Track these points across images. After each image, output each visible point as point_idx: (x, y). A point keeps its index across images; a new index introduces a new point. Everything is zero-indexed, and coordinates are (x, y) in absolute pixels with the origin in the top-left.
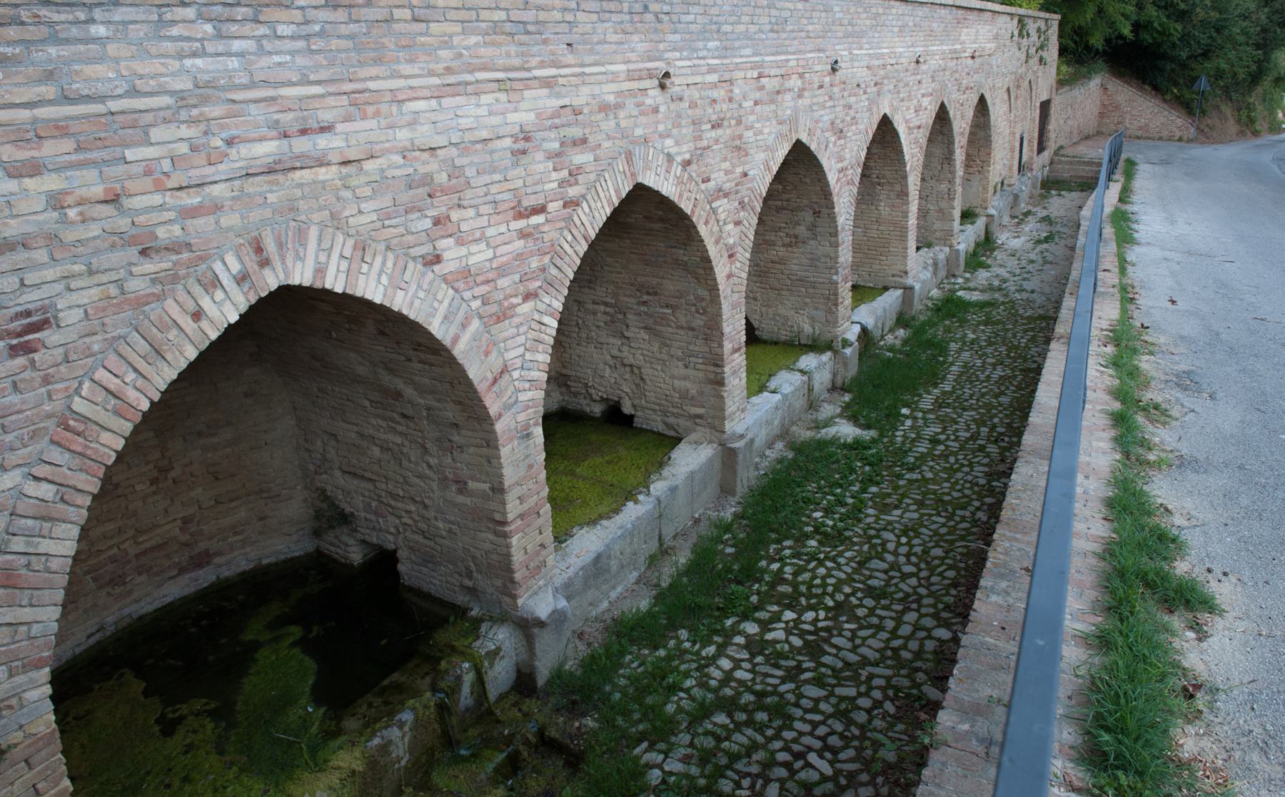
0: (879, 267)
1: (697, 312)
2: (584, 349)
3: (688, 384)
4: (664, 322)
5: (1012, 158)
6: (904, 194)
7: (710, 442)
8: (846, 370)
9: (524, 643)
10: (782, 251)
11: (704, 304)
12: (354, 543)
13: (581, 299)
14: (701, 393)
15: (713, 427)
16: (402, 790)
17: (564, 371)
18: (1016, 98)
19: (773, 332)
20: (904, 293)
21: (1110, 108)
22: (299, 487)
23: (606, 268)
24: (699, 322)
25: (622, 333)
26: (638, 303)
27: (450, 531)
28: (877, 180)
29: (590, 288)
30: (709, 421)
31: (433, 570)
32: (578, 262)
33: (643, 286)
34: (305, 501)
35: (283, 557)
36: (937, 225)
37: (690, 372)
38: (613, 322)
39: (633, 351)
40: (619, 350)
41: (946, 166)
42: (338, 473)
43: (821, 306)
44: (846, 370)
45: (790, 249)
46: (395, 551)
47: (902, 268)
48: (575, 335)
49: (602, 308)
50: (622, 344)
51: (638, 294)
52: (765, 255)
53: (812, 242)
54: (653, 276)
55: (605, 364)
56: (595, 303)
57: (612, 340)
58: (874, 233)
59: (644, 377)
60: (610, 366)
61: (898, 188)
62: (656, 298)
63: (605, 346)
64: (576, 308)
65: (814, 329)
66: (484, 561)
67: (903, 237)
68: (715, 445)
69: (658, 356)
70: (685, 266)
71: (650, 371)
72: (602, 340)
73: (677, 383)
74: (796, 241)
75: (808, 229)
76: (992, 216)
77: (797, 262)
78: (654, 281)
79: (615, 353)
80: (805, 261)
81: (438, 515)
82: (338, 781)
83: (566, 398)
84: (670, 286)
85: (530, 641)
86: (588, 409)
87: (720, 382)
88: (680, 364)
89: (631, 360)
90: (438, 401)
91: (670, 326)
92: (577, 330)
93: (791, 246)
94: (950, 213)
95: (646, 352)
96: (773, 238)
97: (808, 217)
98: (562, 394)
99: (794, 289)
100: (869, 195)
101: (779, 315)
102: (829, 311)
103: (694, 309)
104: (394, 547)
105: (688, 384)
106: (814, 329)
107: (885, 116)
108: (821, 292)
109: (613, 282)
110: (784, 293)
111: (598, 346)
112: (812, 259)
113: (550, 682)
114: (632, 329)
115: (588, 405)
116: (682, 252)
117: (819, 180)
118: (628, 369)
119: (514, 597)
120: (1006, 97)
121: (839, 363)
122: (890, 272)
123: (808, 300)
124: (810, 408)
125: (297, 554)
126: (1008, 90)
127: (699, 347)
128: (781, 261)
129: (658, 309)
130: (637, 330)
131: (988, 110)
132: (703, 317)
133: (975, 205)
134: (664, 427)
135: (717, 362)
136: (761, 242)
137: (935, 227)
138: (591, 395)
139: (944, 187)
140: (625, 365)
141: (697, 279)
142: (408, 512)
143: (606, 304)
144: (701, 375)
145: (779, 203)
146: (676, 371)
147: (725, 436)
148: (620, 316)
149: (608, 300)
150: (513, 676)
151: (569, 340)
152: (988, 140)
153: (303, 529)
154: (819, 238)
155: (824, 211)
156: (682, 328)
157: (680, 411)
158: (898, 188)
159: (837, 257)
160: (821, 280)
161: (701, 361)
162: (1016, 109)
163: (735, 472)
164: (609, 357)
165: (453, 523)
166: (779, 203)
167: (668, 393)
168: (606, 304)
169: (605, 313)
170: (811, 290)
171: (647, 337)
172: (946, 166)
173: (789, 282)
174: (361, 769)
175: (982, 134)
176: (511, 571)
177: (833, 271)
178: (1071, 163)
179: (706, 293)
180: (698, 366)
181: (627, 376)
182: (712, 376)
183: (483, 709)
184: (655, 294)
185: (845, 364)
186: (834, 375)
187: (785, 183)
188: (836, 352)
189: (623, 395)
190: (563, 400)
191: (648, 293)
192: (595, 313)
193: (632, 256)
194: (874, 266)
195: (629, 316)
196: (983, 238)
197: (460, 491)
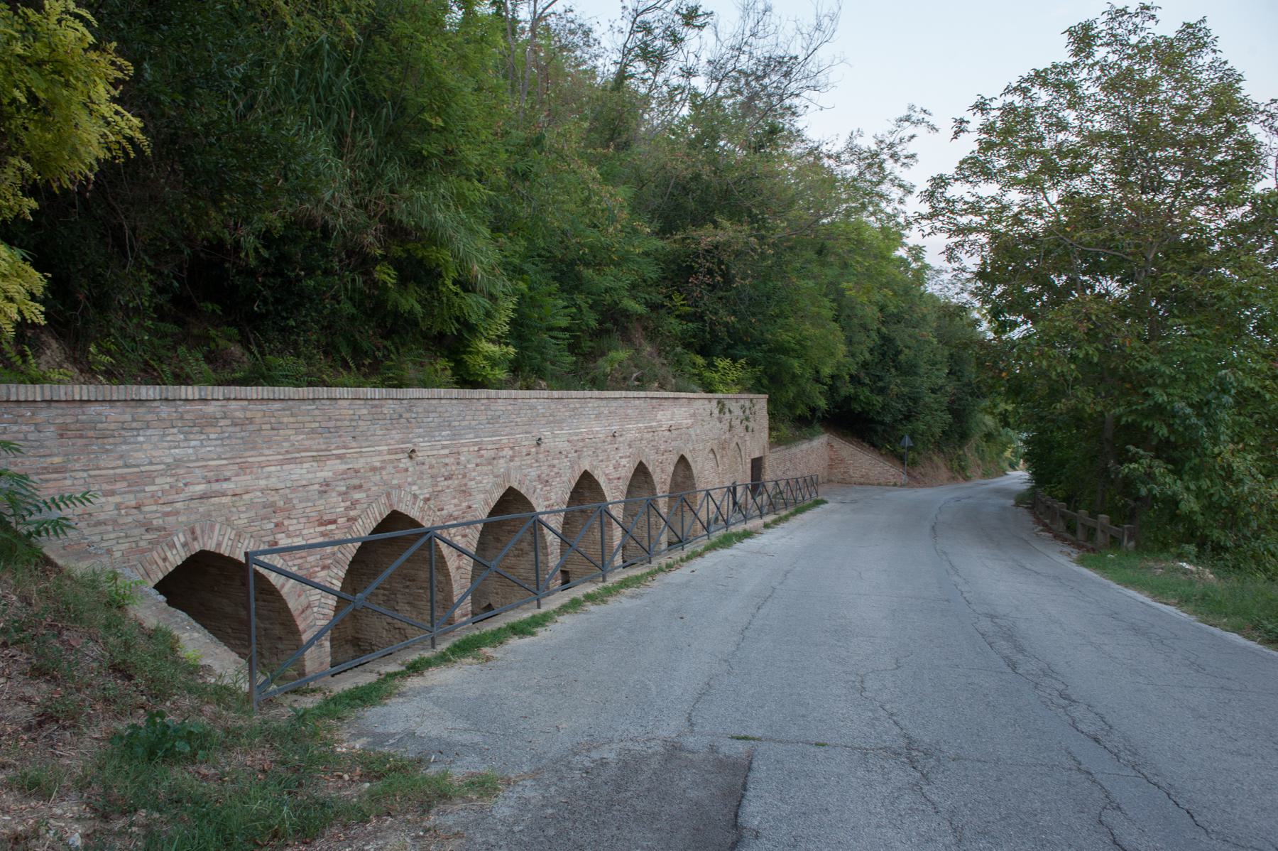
17: (357, 635)
18: (722, 457)
49: (382, 591)
90: (271, 624)
140: (395, 628)
168: (384, 589)
169: (384, 595)
181: (397, 636)
184: (414, 580)
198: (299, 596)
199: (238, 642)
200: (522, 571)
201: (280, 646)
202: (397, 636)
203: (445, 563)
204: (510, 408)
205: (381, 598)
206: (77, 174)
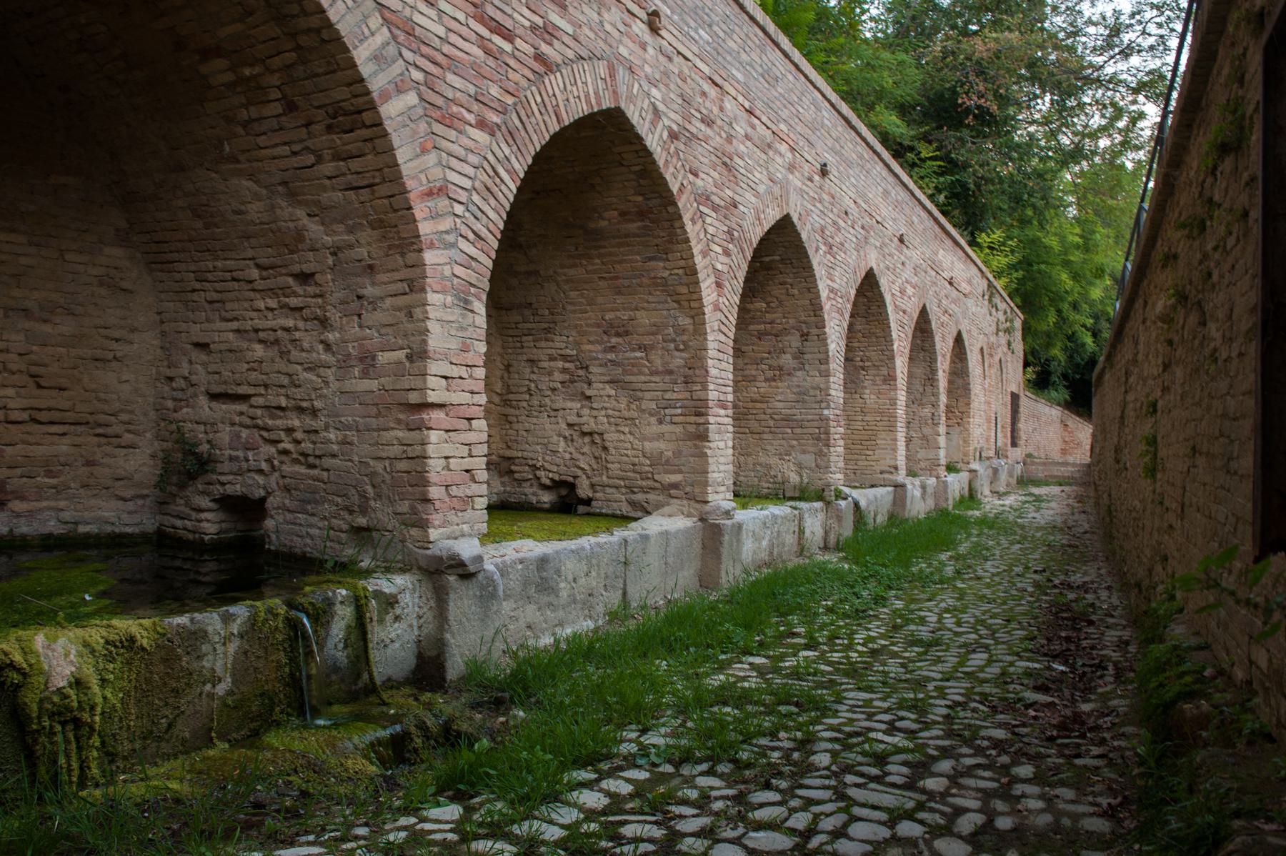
0: (866, 463)
1: (677, 349)
2: (535, 420)
3: (662, 445)
4: (635, 370)
5: (989, 429)
6: (890, 378)
7: (689, 515)
8: (840, 526)
9: (432, 603)
10: (764, 387)
11: (685, 338)
12: (212, 505)
13: (535, 358)
14: (678, 453)
15: (691, 498)
16: (211, 739)
17: (508, 453)
18: (990, 366)
19: (752, 486)
20: (895, 491)
21: (1072, 445)
22: (148, 435)
23: (569, 307)
24: (678, 361)
25: (583, 393)
26: (605, 351)
27: (345, 442)
28: (861, 364)
29: (547, 340)
30: (688, 489)
31: (313, 515)
32: (548, 138)
33: (611, 326)
34: (153, 456)
35: (109, 529)
36: (922, 454)
37: (666, 428)
38: (572, 382)
39: (595, 413)
40: (579, 416)
41: (928, 389)
42: (203, 401)
43: (811, 449)
44: (840, 526)
45: (773, 384)
46: (263, 500)
47: (892, 463)
48: (525, 404)
49: (560, 364)
50: (583, 406)
51: (606, 338)
52: (745, 394)
53: (799, 373)
54: (624, 309)
55: (560, 435)
56: (552, 359)
57: (569, 404)
58: (858, 425)
59: (607, 444)
60: (565, 438)
61: (884, 371)
62: (627, 339)
63: (561, 413)
64: (528, 370)
65: (801, 477)
66: (387, 477)
67: (892, 428)
68: (695, 519)
69: (626, 414)
70: (663, 285)
71: (615, 436)
72: (557, 406)
73: (647, 445)
74: (781, 373)
75: (795, 358)
76: (975, 471)
77: (781, 397)
78: (625, 316)
79: (573, 419)
80: (791, 397)
81: (330, 421)
82: (102, 641)
83: (508, 489)
84: (644, 319)
85: (440, 597)
86: (534, 500)
87: (703, 437)
88: (653, 420)
89: (591, 426)
90: (351, 230)
91: (643, 374)
92: (527, 397)
93: (775, 380)
94: (935, 439)
95: (610, 412)
96: (754, 372)
97: (794, 341)
98: (503, 484)
99: (778, 430)
100: (854, 382)
101: (761, 465)
102: (820, 454)
103: (672, 346)
104: (262, 493)
105: (662, 445)
106: (801, 477)
107: (871, 269)
108: (811, 431)
109: (576, 327)
110: (765, 436)
111: (552, 413)
112: (799, 393)
113: (465, 679)
114: (595, 385)
115: (534, 494)
116: (661, 264)
117: (809, 289)
118: (587, 439)
119: (423, 525)
120: (980, 357)
121: (831, 517)
122: (878, 469)
123: (795, 443)
124: (801, 555)
125: (129, 530)
126: (982, 349)
127: (678, 393)
128: (764, 399)
129: (628, 355)
130: (601, 386)
131: (966, 354)
132: (684, 355)
133: (956, 459)
134: (630, 509)
135: (699, 409)
136: (740, 378)
137: (919, 456)
138: (539, 479)
139: (927, 411)
140: (584, 434)
141: (678, 302)
142: (290, 431)
143: (565, 358)
144: (678, 429)
145: (762, 327)
146: (647, 431)
147: (707, 508)
148: (581, 372)
149: (569, 352)
150: (412, 662)
151: (517, 412)
152: (966, 388)
153: (144, 497)
154: (807, 367)
155: (814, 331)
156: (657, 373)
157: (650, 483)
158: (884, 371)
159: (828, 388)
160: (810, 417)
161: (679, 411)
162: (990, 377)
163: (718, 556)
164: (564, 426)
165: (349, 427)
166: (762, 327)
167: (636, 460)
168: (565, 358)
169: (564, 370)
170: (798, 431)
171: (613, 392)
172: (928, 389)
173: (771, 423)
174: (145, 642)
175: (960, 382)
176: (425, 483)
177: (823, 405)
178: (1044, 464)
179: (689, 321)
180: (676, 419)
181: (586, 449)
182: (692, 429)
183: (360, 684)
184: (627, 333)
185: (839, 519)
186: (826, 533)
187: (769, 299)
188: (828, 503)
189: (579, 473)
190: (505, 492)
191: (618, 335)
192: (550, 374)
193: (601, 283)
194: (860, 463)
195: (592, 369)
196: (967, 494)
197: (365, 375)
198: (424, 151)
199: (272, 303)
200: (781, 405)
201: (369, 291)
202: (586, 449)
203: (697, 283)
204: (791, 78)
205: (558, 376)
206: (135, 439)
